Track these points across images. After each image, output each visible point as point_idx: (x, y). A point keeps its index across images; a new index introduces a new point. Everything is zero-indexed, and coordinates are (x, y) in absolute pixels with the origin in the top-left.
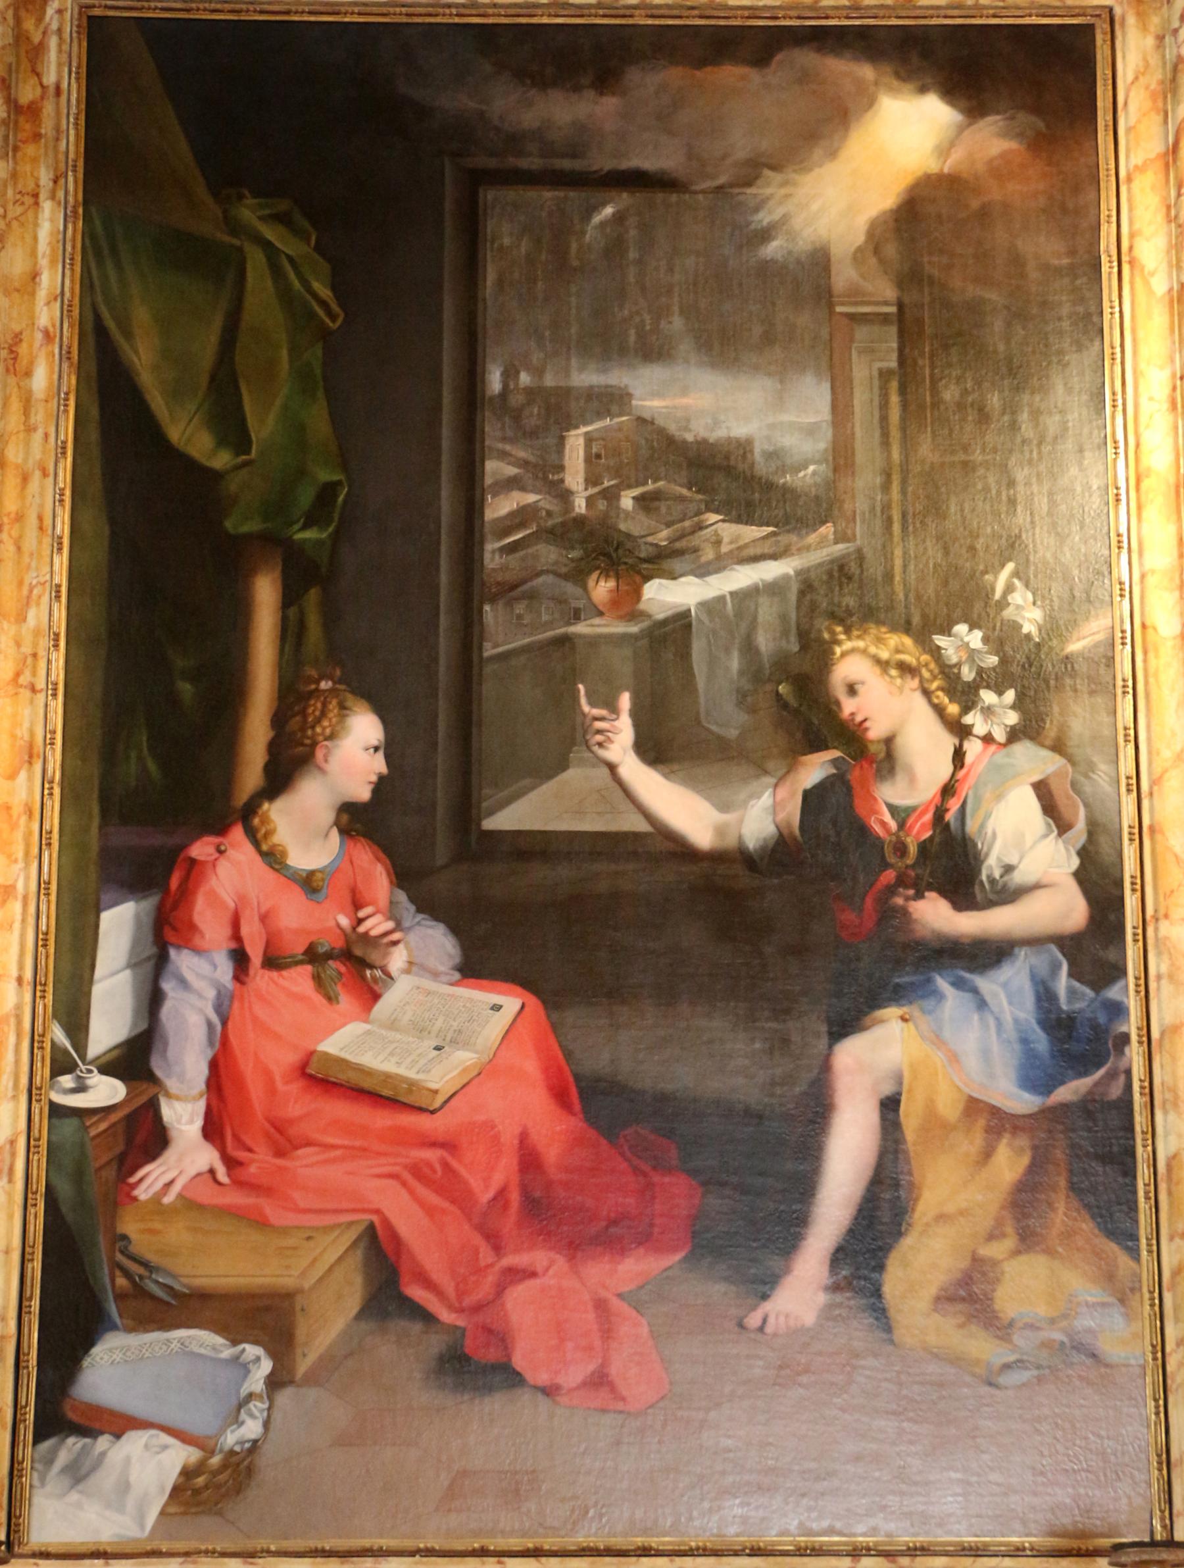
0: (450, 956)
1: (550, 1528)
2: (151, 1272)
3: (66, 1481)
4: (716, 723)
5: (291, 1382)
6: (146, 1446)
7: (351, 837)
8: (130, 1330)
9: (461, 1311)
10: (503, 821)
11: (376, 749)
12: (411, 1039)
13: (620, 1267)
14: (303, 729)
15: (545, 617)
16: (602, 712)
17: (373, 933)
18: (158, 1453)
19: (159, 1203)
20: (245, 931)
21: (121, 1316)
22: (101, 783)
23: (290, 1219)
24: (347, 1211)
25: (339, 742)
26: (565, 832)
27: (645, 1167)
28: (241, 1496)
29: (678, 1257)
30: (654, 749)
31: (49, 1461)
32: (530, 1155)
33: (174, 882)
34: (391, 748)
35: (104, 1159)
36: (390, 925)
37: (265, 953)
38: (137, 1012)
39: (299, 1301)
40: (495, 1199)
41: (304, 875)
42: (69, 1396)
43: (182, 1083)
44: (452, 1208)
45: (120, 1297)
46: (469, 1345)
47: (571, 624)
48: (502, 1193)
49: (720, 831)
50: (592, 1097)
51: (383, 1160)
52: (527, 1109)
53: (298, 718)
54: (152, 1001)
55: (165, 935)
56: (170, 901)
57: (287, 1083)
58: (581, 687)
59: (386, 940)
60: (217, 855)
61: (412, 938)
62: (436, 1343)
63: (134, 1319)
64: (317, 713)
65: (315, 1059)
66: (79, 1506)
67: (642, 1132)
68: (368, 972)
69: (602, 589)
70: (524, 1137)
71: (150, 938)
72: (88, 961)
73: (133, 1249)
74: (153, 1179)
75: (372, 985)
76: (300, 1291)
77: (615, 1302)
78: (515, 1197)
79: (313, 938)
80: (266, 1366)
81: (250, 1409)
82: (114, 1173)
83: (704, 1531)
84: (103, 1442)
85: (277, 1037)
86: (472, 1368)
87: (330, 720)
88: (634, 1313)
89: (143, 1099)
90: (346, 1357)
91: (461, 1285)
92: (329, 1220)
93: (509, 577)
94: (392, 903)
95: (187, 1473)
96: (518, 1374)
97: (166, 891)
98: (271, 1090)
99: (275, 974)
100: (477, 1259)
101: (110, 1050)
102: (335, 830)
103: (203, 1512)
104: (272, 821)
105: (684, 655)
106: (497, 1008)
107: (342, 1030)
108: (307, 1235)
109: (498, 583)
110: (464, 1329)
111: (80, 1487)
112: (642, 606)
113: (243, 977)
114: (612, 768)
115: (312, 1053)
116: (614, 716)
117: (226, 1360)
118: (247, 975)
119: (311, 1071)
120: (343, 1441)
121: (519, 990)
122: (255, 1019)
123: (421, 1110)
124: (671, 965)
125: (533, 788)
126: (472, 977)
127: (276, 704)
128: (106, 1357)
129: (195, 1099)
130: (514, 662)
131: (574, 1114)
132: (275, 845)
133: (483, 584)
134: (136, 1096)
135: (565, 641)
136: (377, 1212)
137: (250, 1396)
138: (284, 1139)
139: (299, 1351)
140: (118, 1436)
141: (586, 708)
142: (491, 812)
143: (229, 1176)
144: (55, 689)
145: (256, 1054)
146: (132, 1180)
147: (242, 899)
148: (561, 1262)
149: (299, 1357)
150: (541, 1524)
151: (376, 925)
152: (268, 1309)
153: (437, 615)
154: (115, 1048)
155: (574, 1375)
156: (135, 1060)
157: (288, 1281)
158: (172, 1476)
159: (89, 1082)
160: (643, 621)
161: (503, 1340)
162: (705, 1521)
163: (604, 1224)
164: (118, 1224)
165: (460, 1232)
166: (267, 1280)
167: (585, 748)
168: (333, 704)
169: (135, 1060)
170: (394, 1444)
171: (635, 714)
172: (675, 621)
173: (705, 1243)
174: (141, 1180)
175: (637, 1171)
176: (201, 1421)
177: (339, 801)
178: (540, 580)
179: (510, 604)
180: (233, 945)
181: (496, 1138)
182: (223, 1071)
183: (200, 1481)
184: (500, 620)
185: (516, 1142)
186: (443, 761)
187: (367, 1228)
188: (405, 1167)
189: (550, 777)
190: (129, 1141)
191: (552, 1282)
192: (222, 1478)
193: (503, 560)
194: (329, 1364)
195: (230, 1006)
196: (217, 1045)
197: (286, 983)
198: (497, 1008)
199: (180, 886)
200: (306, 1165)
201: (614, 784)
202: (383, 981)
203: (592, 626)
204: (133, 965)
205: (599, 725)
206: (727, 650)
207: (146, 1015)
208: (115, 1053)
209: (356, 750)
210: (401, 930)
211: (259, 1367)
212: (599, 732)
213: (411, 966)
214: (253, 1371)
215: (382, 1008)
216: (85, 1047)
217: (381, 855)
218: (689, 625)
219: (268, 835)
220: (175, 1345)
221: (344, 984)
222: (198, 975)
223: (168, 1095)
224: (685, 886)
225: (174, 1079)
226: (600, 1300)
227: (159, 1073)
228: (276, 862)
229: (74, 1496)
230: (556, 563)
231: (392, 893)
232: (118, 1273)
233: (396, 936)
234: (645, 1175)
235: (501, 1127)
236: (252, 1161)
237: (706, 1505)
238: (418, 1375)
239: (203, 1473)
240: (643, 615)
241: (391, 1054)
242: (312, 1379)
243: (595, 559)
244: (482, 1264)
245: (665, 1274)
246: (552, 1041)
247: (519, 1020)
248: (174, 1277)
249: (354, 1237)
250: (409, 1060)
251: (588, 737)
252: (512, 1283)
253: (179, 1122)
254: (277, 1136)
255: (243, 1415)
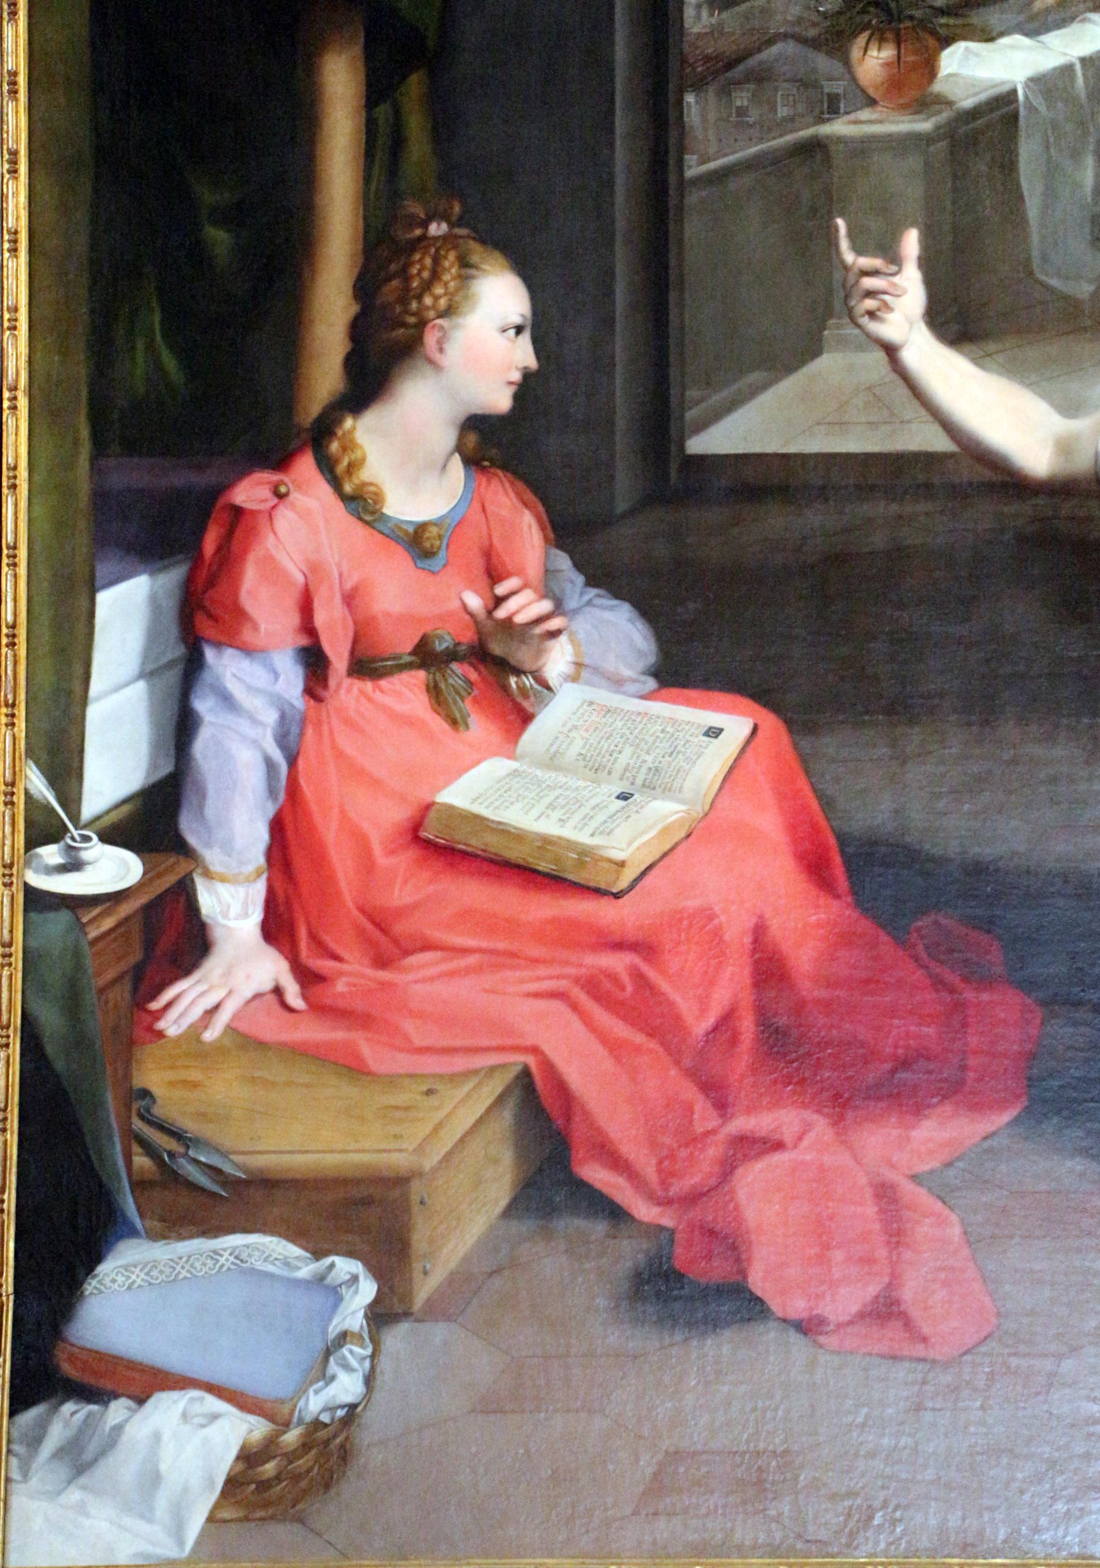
0: (641, 654)
1: (816, 1541)
2: (188, 1147)
3: (63, 1471)
4: (1059, 275)
5: (407, 1314)
6: (185, 1417)
7: (484, 469)
8: (155, 1236)
9: (665, 1202)
10: (719, 439)
11: (519, 329)
12: (581, 783)
13: (914, 1133)
14: (403, 300)
15: (782, 112)
16: (876, 262)
17: (519, 619)
18: (203, 1426)
19: (199, 1040)
20: (320, 619)
21: (142, 1216)
22: (91, 392)
23: (403, 1063)
24: (488, 1049)
25: (460, 320)
26: (817, 455)
27: (953, 979)
28: (333, 1492)
29: (1006, 1117)
30: (957, 320)
31: (35, 1441)
32: (770, 959)
33: (210, 543)
34: (541, 328)
35: (110, 974)
36: (546, 606)
37: (352, 652)
38: (156, 747)
39: (416, 1188)
40: (715, 1029)
41: (411, 530)
42: (64, 1340)
43: (229, 856)
44: (653, 1045)
45: (140, 1185)
46: (680, 1256)
47: (823, 121)
48: (727, 1019)
49: (1064, 447)
50: (857, 865)
51: (542, 971)
52: (764, 890)
53: (395, 283)
54: (180, 729)
55: (199, 624)
56: (203, 574)
57: (392, 852)
58: (840, 222)
59: (538, 630)
60: (276, 501)
61: (582, 625)
62: (630, 1252)
63: (162, 1220)
64: (426, 274)
65: (432, 814)
66: (81, 1509)
67: (943, 921)
68: (513, 681)
69: (873, 61)
70: (759, 932)
71: (174, 631)
72: (78, 669)
73: (159, 1111)
74: (188, 1004)
75: (519, 699)
76: (418, 1174)
77: (908, 1188)
78: (747, 1026)
79: (427, 628)
80: (368, 1290)
81: (344, 1358)
82: (127, 996)
83: (1059, 1550)
84: (118, 1410)
85: (375, 783)
86: (686, 1291)
87: (446, 284)
88: (939, 1205)
89: (170, 880)
90: (490, 1275)
91: (666, 1163)
92: (460, 1063)
93: (726, 47)
94: (548, 573)
95: (249, 1457)
96: (759, 1301)
97: (197, 560)
98: (367, 864)
99: (368, 686)
100: (691, 1122)
101: (117, 806)
102: (457, 457)
103: (272, 1518)
104: (361, 447)
105: (1008, 166)
106: (714, 733)
107: (474, 772)
108: (425, 1088)
109: (707, 59)
110: (672, 1232)
111: (83, 1480)
112: (938, 87)
113: (319, 691)
114: (891, 350)
115: (429, 806)
116: (894, 268)
117: (307, 1282)
118: (325, 686)
119: (424, 834)
120: (489, 1406)
121: (746, 702)
122: (340, 755)
123: (598, 892)
124: (988, 661)
125: (765, 387)
126: (674, 685)
127: (360, 261)
128: (120, 1279)
129: (249, 880)
130: (733, 185)
131: (838, 897)
132: (365, 484)
133: (683, 61)
134: (159, 875)
135: (814, 148)
136: (535, 1050)
137: (344, 1337)
138: (388, 941)
139: (417, 1266)
140: (141, 1401)
141: (849, 257)
142: (701, 426)
143: (305, 997)
144: (15, 241)
145: (342, 812)
146: (155, 1006)
147: (315, 569)
148: (821, 1126)
149: (417, 1275)
150: (799, 1536)
151: (525, 606)
152: (367, 1202)
153: (611, 112)
154: (125, 802)
155: (846, 1301)
156: (155, 821)
157: (399, 1161)
158: (225, 1462)
159: (85, 855)
160: (940, 112)
161: (734, 1247)
162: (1060, 1533)
163: (888, 1066)
164: (135, 1073)
165: (662, 1080)
166: (366, 1158)
167: (847, 320)
168: (450, 259)
169: (155, 821)
170: (568, 1411)
171: (927, 264)
172: (991, 111)
173: (1048, 1095)
174: (169, 1005)
175: (938, 984)
176: (268, 1376)
177: (461, 414)
178: (775, 49)
179: (725, 92)
180: (304, 641)
181: (717, 934)
182: (290, 834)
183: (269, 1468)
184: (712, 116)
185: (748, 940)
186: (622, 346)
187: (517, 1077)
188: (577, 980)
189: (790, 369)
190: (149, 944)
191: (808, 1157)
192: (302, 1463)
193: (713, 21)
194: (463, 1285)
195: (302, 734)
196: (282, 796)
197: (388, 700)
198: (714, 733)
199: (219, 549)
200: (421, 979)
201: (893, 376)
202: (536, 694)
203: (855, 122)
204: (149, 674)
205: (868, 283)
206: (1076, 155)
207: (172, 752)
208: (126, 808)
209: (487, 332)
210: (564, 614)
211: (356, 1292)
212: (870, 294)
213: (579, 670)
214: (347, 1297)
215: (534, 735)
216: (79, 800)
217: (529, 496)
218: (1015, 117)
219: (352, 468)
220: (226, 1259)
221: (476, 701)
222: (250, 688)
223: (207, 874)
224: (1008, 536)
225: (216, 850)
226: (883, 1185)
227: (192, 840)
228: (366, 510)
229: (74, 1495)
230: (799, 21)
231: (547, 555)
232: (136, 1148)
233: (554, 624)
234: (952, 991)
235: (723, 918)
236: (341, 974)
237: (1061, 1507)
238: (601, 1302)
239: (274, 1457)
240: (943, 102)
241: (551, 806)
242: (434, 1311)
243: (864, 11)
244: (699, 1129)
245: (986, 1144)
246: (802, 783)
247: (749, 750)
248: (224, 1154)
249: (499, 1090)
250: (578, 817)
251: (853, 303)
252: (746, 1158)
253: (225, 916)
254: (377, 934)
255: (333, 1367)
